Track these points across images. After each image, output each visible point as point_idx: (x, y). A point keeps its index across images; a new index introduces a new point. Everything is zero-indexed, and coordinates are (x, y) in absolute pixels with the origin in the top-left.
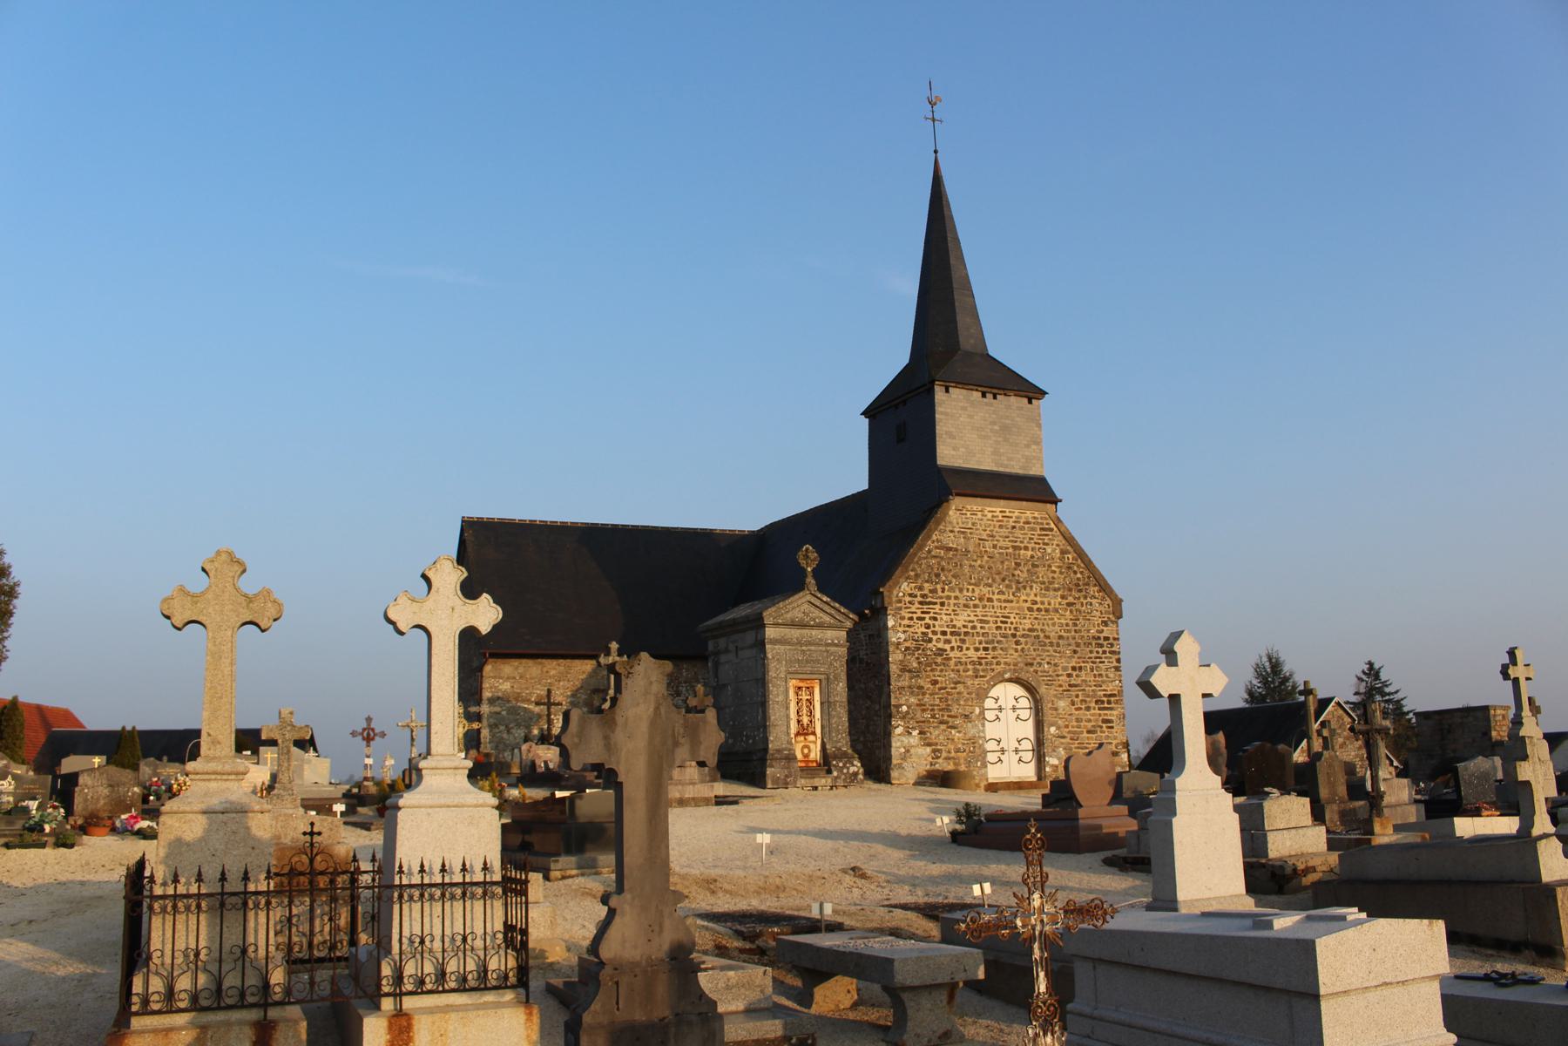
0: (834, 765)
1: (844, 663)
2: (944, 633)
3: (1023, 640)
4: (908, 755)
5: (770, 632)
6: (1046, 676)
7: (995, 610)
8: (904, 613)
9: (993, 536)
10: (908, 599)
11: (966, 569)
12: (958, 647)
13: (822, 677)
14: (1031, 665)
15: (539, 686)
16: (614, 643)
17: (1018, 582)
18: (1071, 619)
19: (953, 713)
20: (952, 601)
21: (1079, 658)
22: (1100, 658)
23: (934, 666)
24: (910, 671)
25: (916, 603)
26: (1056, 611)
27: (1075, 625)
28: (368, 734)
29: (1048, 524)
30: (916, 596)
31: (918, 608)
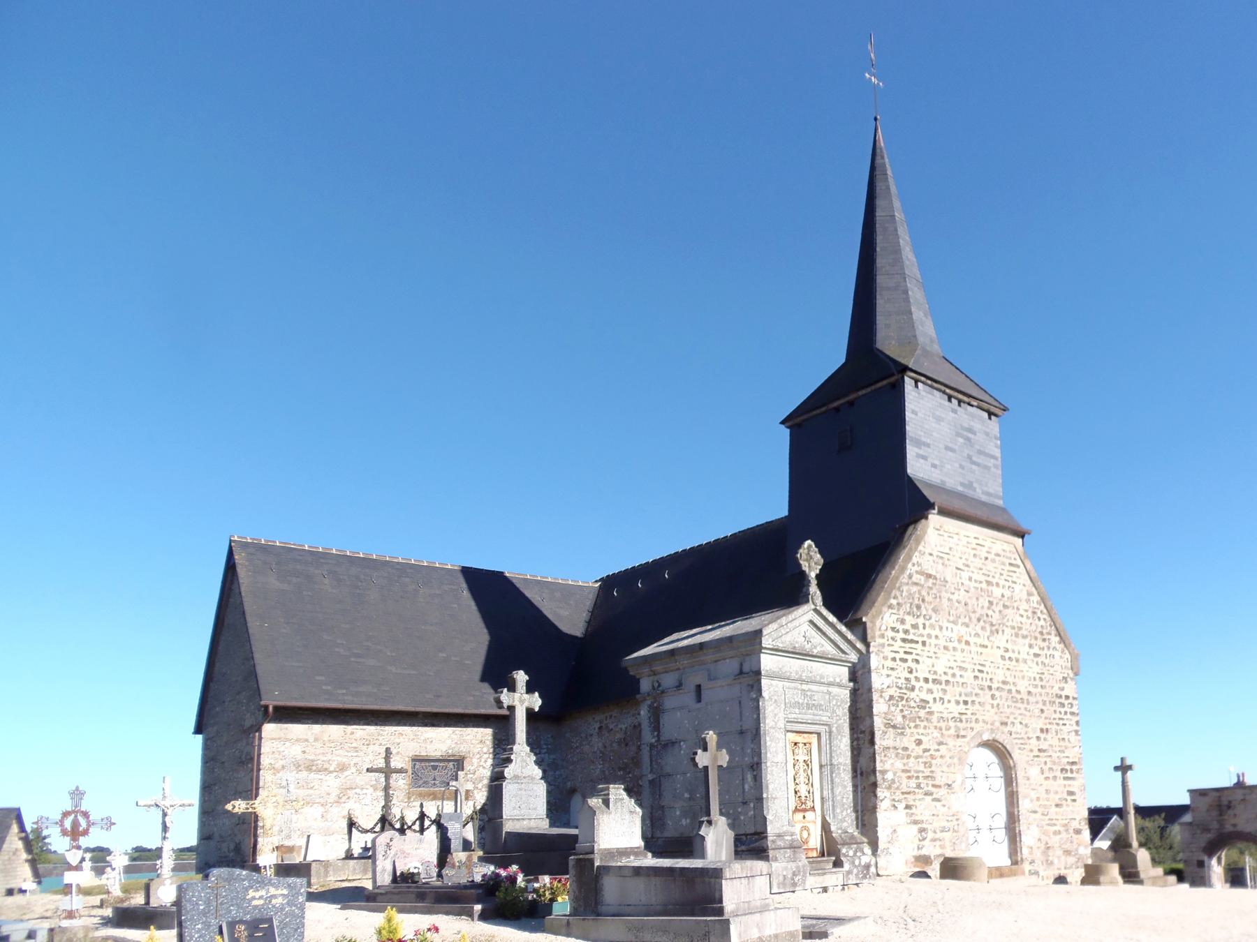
0: (844, 854)
1: (846, 711)
2: (926, 680)
3: (997, 694)
4: (895, 836)
5: (768, 662)
6: (1019, 739)
7: (972, 655)
8: (887, 650)
9: (968, 566)
10: (890, 634)
11: (945, 602)
12: (941, 699)
13: (822, 729)
14: (1006, 724)
15: (341, 752)
16: (521, 673)
17: (992, 625)
18: (1038, 673)
19: (937, 783)
20: (933, 641)
21: (1046, 718)
22: (1062, 719)
23: (918, 722)
24: (894, 727)
25: (899, 641)
26: (1025, 661)
27: (1041, 679)
28: (75, 824)
29: (1015, 559)
30: (898, 631)
31: (901, 647)
